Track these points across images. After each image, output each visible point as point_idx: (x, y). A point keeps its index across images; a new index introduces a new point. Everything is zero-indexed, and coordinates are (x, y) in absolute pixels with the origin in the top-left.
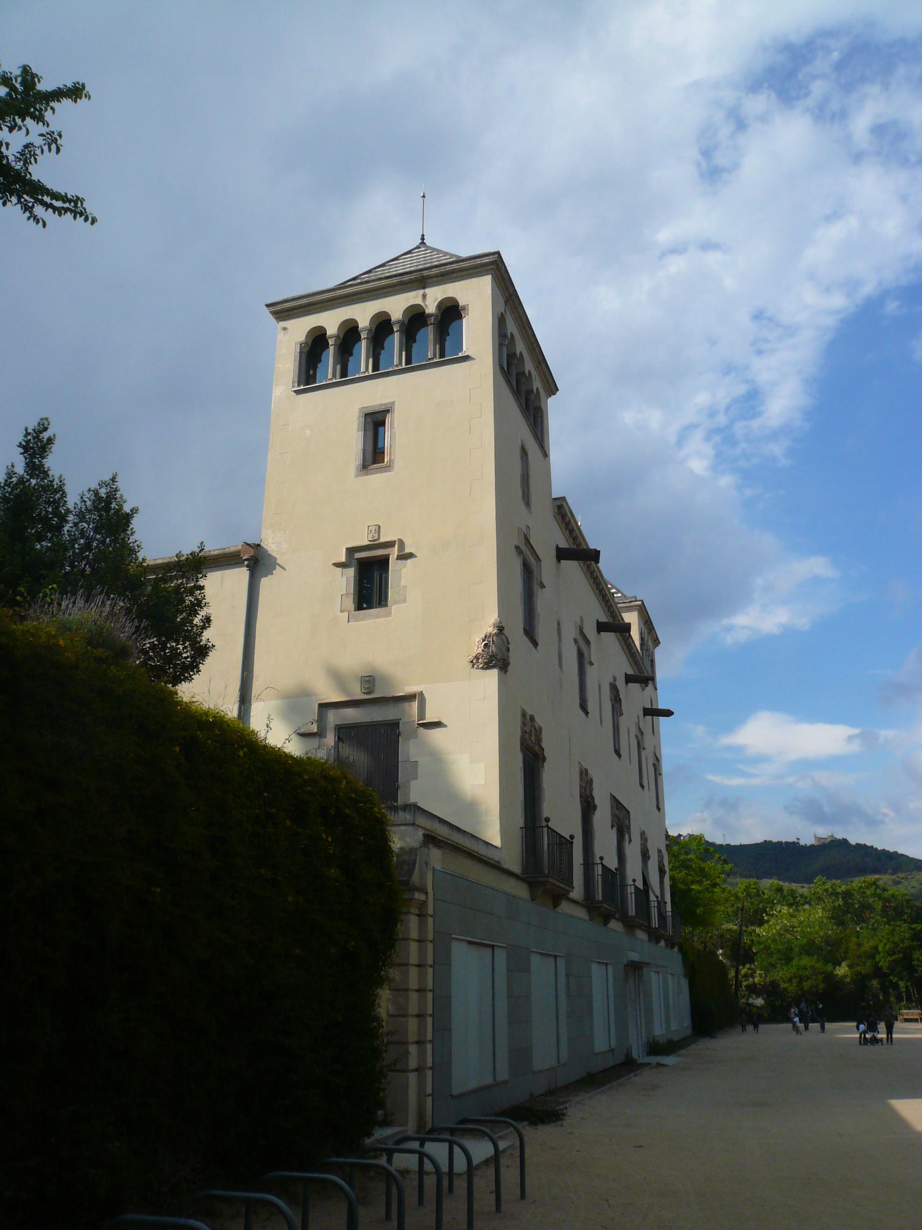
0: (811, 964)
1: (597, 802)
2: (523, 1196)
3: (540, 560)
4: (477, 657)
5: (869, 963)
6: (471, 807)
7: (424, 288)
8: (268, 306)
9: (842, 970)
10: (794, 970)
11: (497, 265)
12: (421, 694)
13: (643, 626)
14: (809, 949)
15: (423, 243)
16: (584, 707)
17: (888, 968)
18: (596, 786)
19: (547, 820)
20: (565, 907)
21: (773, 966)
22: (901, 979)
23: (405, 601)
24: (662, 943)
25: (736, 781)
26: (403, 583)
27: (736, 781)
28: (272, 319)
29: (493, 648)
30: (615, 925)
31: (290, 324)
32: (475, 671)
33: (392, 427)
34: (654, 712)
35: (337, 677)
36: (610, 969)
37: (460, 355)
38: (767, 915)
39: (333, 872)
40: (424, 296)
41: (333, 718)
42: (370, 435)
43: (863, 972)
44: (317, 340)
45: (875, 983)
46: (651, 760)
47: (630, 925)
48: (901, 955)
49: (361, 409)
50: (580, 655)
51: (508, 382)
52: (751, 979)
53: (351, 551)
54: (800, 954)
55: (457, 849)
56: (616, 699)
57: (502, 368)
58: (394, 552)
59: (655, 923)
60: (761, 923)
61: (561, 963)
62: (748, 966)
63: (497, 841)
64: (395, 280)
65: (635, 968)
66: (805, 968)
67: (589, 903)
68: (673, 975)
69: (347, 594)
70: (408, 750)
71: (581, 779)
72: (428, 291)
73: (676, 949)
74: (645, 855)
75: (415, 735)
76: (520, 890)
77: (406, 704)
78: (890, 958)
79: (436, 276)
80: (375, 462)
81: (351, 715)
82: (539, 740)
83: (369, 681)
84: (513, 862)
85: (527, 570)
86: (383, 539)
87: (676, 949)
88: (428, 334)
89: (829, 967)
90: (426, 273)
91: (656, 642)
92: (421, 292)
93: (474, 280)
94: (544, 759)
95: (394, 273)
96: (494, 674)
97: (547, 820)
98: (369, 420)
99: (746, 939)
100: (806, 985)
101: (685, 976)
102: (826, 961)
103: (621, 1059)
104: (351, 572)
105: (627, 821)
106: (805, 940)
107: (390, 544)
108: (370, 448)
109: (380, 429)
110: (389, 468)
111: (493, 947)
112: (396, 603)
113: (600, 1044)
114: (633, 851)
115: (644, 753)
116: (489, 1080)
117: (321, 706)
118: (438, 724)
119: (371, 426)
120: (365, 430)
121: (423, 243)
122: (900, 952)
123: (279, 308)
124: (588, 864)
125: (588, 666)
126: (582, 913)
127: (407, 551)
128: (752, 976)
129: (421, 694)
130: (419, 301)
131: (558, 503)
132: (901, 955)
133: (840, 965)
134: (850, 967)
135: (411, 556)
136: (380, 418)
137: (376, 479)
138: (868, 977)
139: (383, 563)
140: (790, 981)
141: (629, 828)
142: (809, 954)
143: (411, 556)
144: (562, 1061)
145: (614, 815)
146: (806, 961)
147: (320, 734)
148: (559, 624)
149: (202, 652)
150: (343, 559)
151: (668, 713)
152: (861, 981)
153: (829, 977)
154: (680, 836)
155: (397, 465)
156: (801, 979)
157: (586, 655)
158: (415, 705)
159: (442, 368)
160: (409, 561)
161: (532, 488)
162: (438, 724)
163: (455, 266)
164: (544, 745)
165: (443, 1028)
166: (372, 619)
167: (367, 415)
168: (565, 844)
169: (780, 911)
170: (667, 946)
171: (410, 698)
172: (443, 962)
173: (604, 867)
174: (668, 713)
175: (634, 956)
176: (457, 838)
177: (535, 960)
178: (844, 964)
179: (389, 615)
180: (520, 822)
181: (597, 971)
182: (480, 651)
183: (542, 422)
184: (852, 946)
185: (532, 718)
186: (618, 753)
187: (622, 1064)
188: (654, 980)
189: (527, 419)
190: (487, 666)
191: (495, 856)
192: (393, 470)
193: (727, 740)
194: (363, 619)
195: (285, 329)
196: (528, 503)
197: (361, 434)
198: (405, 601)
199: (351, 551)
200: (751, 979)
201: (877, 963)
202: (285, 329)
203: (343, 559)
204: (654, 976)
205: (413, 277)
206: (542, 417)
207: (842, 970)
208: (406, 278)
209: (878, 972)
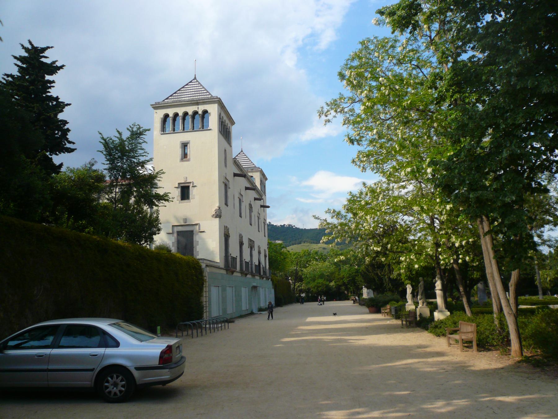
0: (321, 282)
1: (244, 242)
2: (228, 328)
3: (229, 181)
4: (213, 215)
5: (341, 281)
6: (212, 253)
7: (198, 105)
8: (151, 105)
9: (332, 284)
10: (315, 284)
11: (219, 102)
12: (199, 224)
13: (261, 176)
14: (322, 276)
15: (195, 78)
16: (241, 216)
17: (347, 282)
18: (243, 238)
19: (231, 254)
20: (235, 274)
21: (309, 282)
22: (351, 286)
23: (194, 198)
24: (265, 279)
25: (309, 201)
26: (194, 194)
27: (309, 201)
28: (152, 109)
29: (217, 213)
30: (249, 276)
31: (158, 111)
32: (213, 218)
33: (190, 148)
34: (264, 207)
35: (177, 219)
36: (247, 289)
37: (209, 129)
38: (308, 264)
39: (195, 277)
40: (198, 108)
41: (176, 229)
42: (183, 149)
43: (339, 284)
44: (166, 116)
45: (343, 288)
46: (263, 221)
47: (253, 275)
48: (351, 278)
49: (181, 142)
50: (240, 200)
51: (221, 134)
52: (300, 287)
53: (179, 184)
54: (318, 278)
55: (211, 266)
56: (251, 206)
57: (220, 131)
58: (191, 185)
59: (262, 274)
60: (306, 267)
61: (234, 288)
62: (300, 283)
63: (218, 261)
64: (189, 102)
65: (255, 288)
66: (319, 283)
67: (242, 272)
68: (268, 288)
69: (178, 196)
70: (196, 238)
71: (239, 237)
72: (199, 106)
73: (270, 280)
74: (259, 253)
75: (197, 234)
76: (224, 272)
77: (195, 226)
78: (348, 279)
79: (202, 102)
80: (185, 158)
81: (181, 229)
82: (228, 232)
83: (185, 220)
84: (222, 265)
85: (226, 185)
86: (188, 181)
87: (270, 280)
88: (198, 118)
89: (327, 283)
90: (199, 101)
91: (266, 179)
92: (197, 106)
93: (212, 105)
94: (230, 237)
95: (188, 98)
96: (218, 219)
97: (231, 254)
98: (183, 145)
99: (300, 273)
100: (320, 289)
101: (273, 288)
102: (327, 280)
103: (249, 312)
104: (179, 190)
105: (253, 245)
106: (320, 273)
107: (190, 183)
108: (183, 153)
109: (186, 147)
110: (189, 160)
111: (219, 286)
112: (192, 199)
113: (244, 308)
114: (255, 253)
115: (260, 221)
116: (218, 315)
117: (173, 226)
118: (204, 232)
119: (183, 147)
120: (182, 148)
121: (195, 78)
122: (351, 277)
123: (154, 106)
124: (241, 261)
125: (242, 203)
126: (239, 275)
127: (195, 185)
128: (301, 286)
129: (199, 224)
130: (196, 109)
131: (234, 160)
132: (351, 278)
133: (332, 282)
134: (335, 282)
135: (195, 186)
136: (186, 144)
137: (185, 163)
138: (341, 286)
139: (188, 187)
140: (314, 288)
141: (254, 246)
142: (321, 278)
143: (195, 186)
144: (234, 312)
145: (249, 244)
146: (320, 281)
147: (172, 233)
148: (234, 195)
149: (159, 230)
150: (177, 186)
151: (268, 207)
152: (338, 287)
153: (327, 286)
154: (284, 225)
155: (191, 159)
156: (318, 287)
157: (242, 200)
158: (198, 226)
159: (224, 245)
160: (195, 188)
161: (227, 161)
162: (204, 232)
163: (207, 100)
164: (229, 233)
165: (210, 304)
166: (185, 203)
167: (182, 143)
168: (234, 259)
169: (313, 263)
170: (266, 280)
171: (196, 225)
172: (210, 291)
173: (245, 261)
174: (268, 207)
175: (255, 284)
176: (211, 263)
177: (228, 288)
178: (333, 282)
179: (190, 202)
180: (224, 255)
181: (243, 290)
182: (214, 213)
183: (230, 136)
184: (336, 275)
185: (227, 227)
186: (251, 225)
187: (250, 313)
188: (261, 291)
189: (226, 140)
190: (216, 217)
191: (218, 265)
192: (175, 113)
193: (305, 183)
194: (183, 203)
195: (156, 113)
196: (226, 166)
197: (181, 149)
198: (194, 198)
199: (179, 184)
200: (300, 287)
201: (344, 281)
202: (156, 113)
203: (177, 186)
204: (261, 289)
205: (195, 102)
206: (230, 134)
207: (332, 284)
208: (193, 102)
209: (344, 284)
